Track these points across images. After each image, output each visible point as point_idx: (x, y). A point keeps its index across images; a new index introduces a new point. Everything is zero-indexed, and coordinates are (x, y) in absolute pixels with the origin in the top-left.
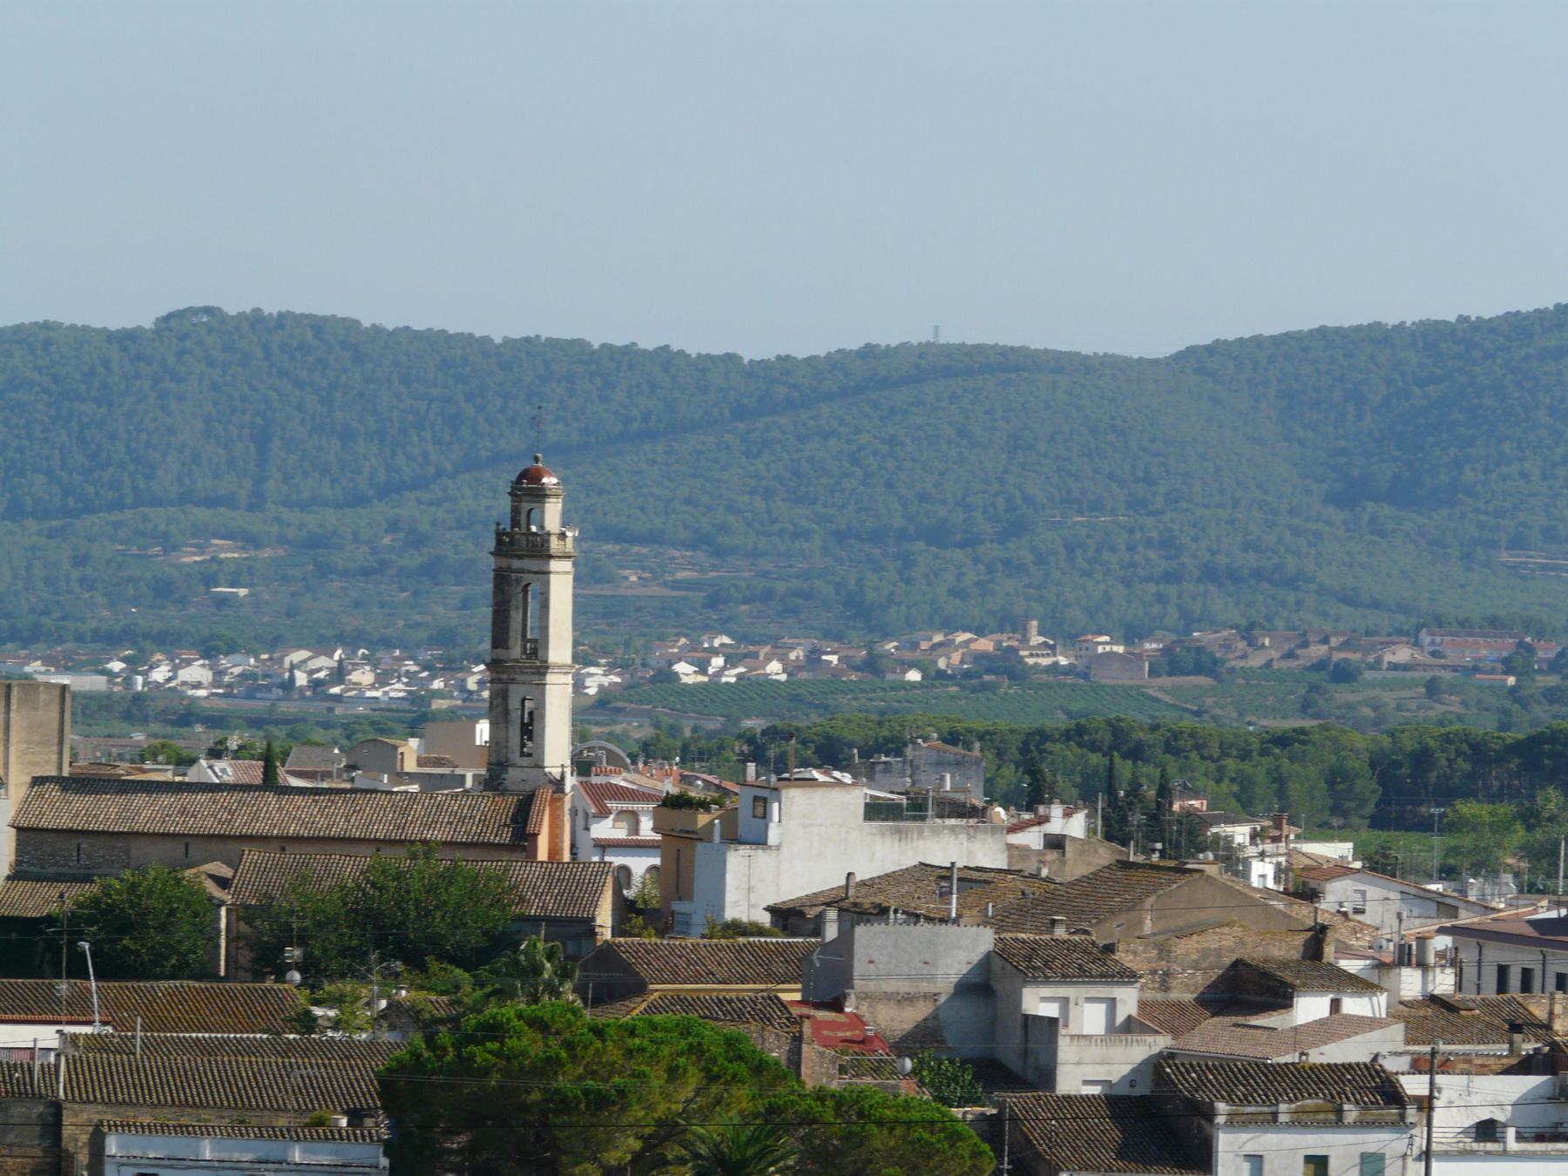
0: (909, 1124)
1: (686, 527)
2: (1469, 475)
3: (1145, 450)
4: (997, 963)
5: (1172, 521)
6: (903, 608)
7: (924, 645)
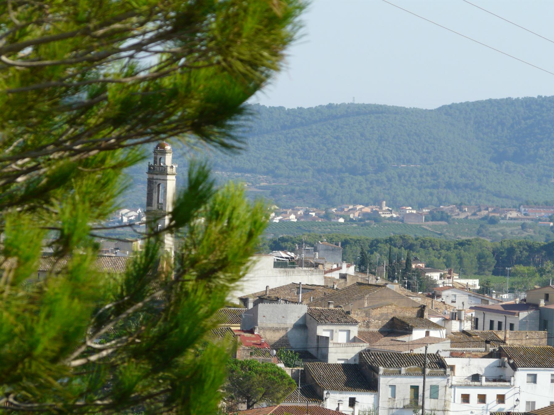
0: (266, 373)
1: (264, 167)
2: (541, 152)
3: (427, 142)
4: (308, 317)
5: (436, 167)
6: (340, 197)
7: (346, 210)
